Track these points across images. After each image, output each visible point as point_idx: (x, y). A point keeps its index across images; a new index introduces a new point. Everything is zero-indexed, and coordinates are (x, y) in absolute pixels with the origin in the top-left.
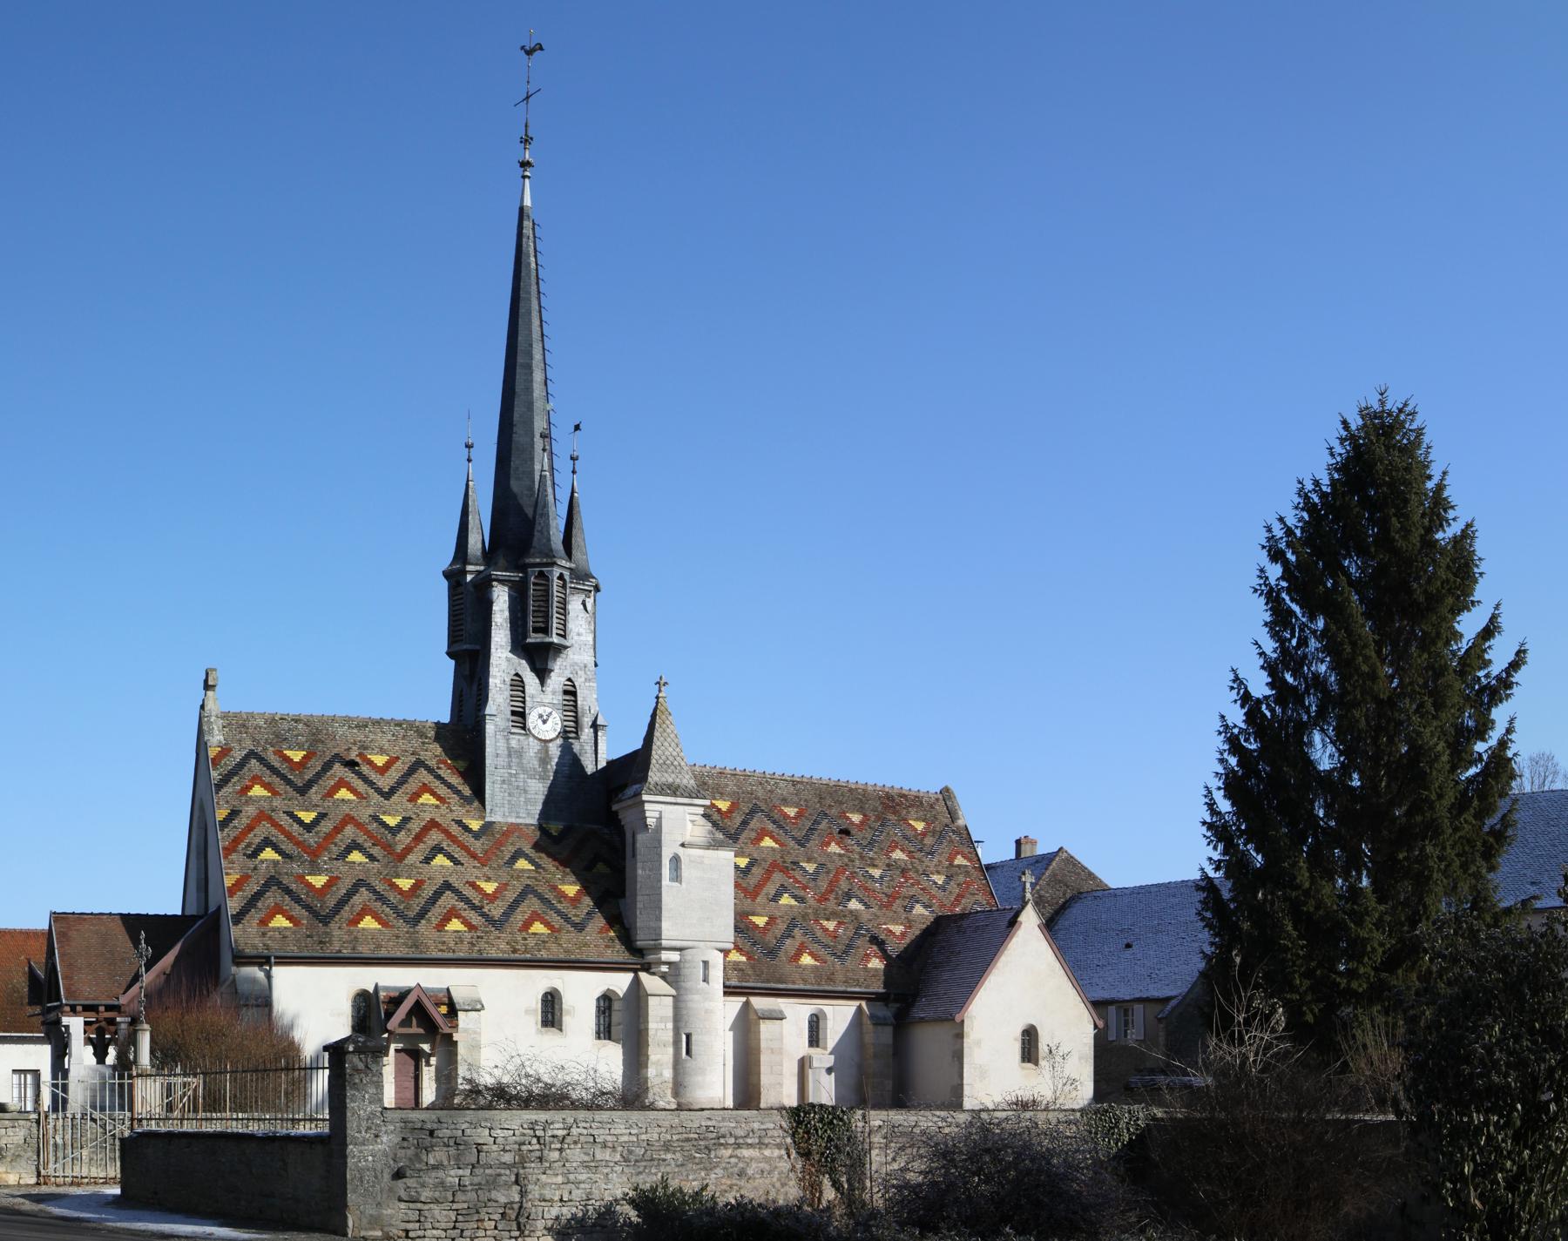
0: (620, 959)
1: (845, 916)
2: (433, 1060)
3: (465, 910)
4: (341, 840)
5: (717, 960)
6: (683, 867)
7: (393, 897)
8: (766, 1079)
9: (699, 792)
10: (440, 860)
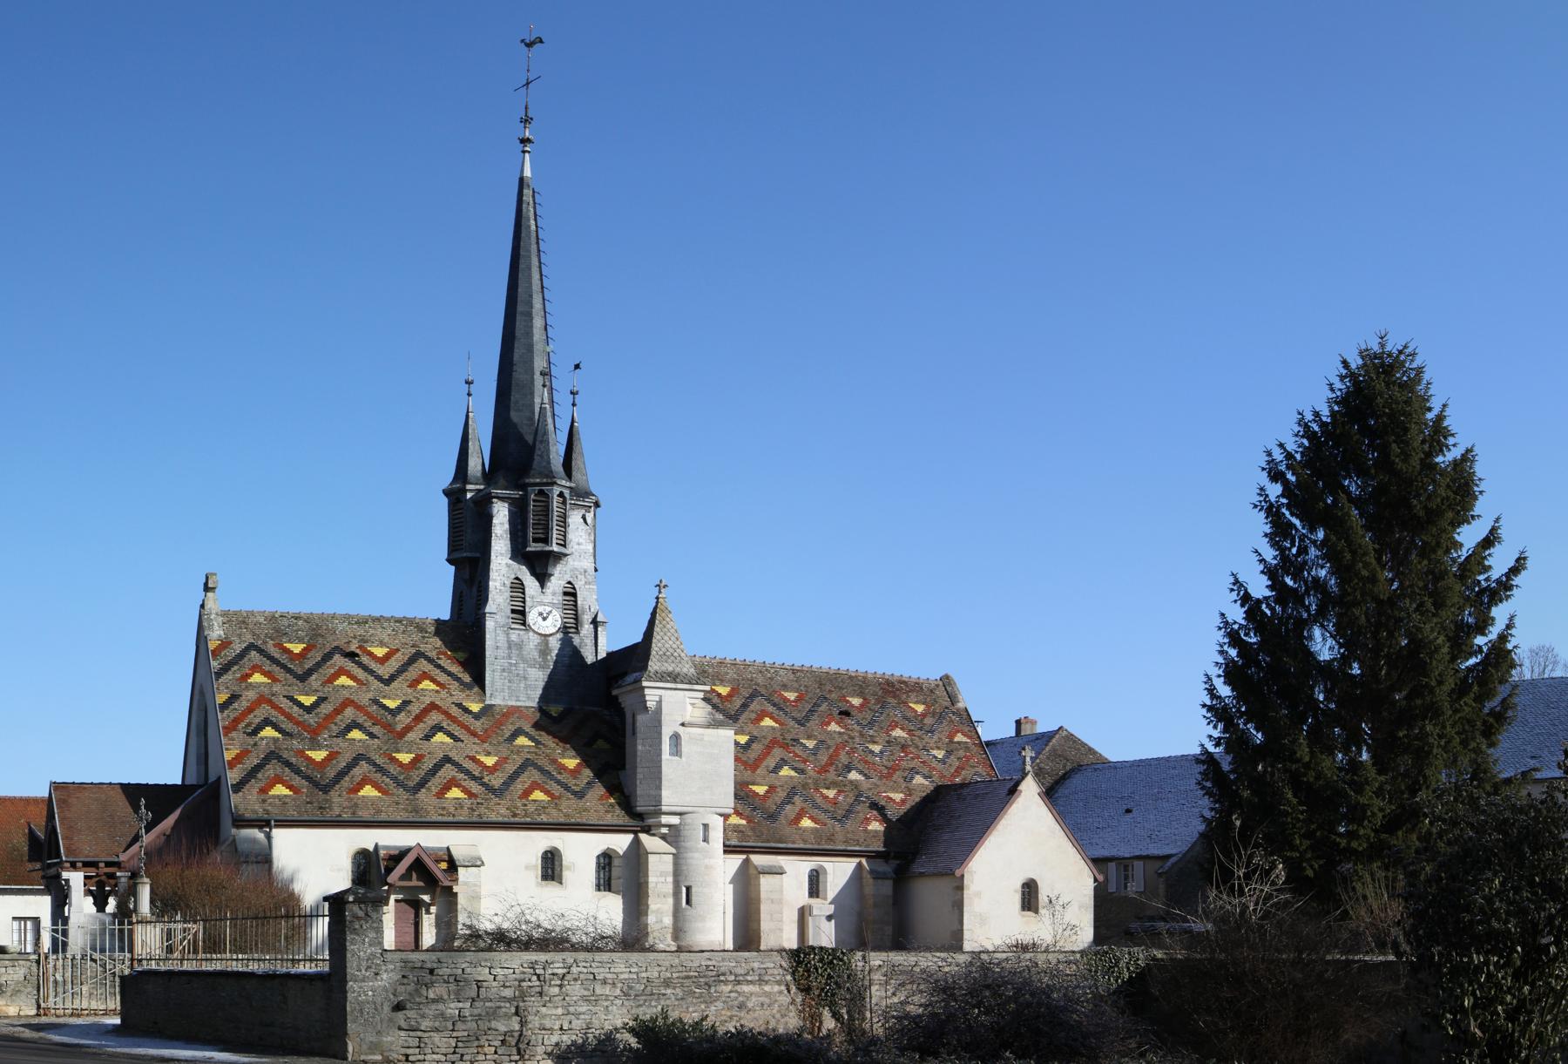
1: (845, 785)
2: (433, 909)
3: (465, 780)
4: (341, 721)
7: (393, 769)
9: (699, 679)
10: (440, 737)
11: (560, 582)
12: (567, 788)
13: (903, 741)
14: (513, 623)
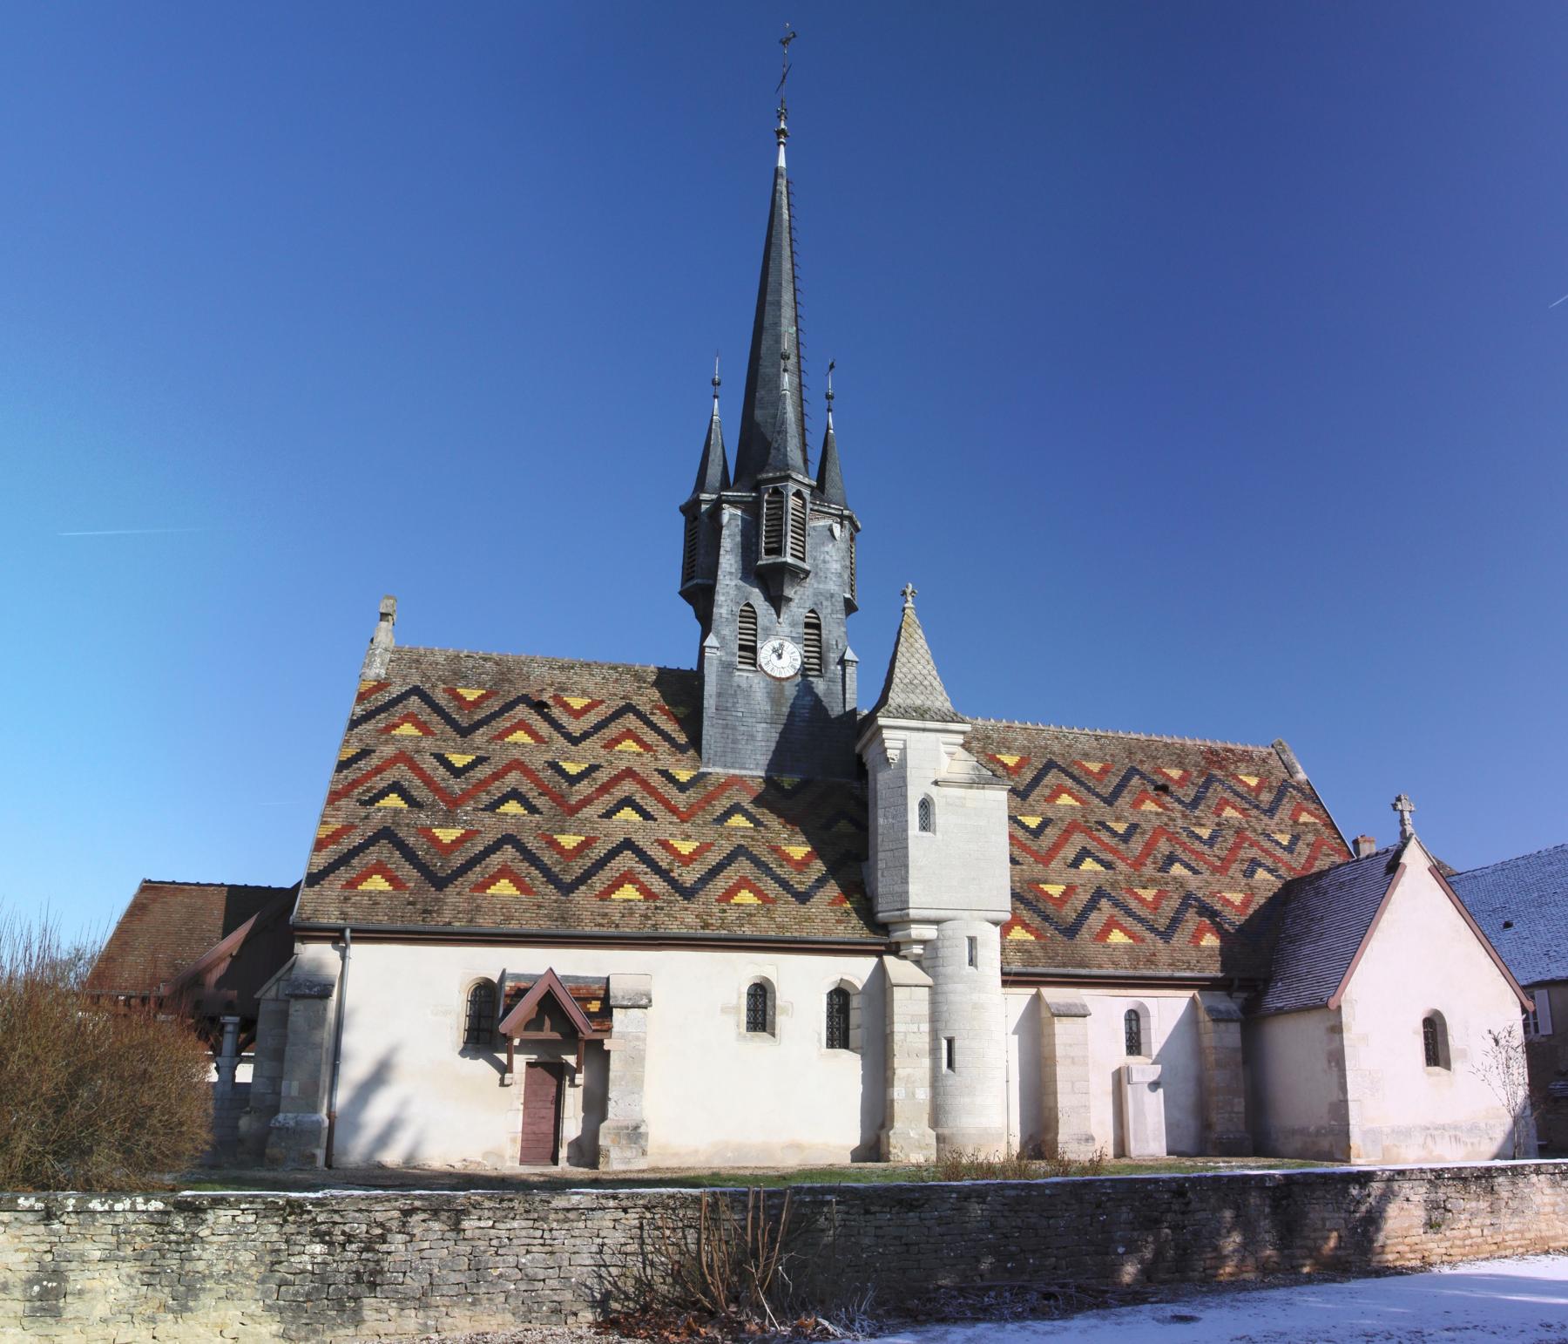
0: (856, 937)
1: (1167, 883)
2: (580, 1079)
3: (646, 874)
4: (498, 788)
5: (991, 940)
6: (937, 811)
8: (1064, 1101)
9: (956, 715)
11: (801, 610)
12: (784, 884)
13: (1237, 824)
14: (740, 662)
